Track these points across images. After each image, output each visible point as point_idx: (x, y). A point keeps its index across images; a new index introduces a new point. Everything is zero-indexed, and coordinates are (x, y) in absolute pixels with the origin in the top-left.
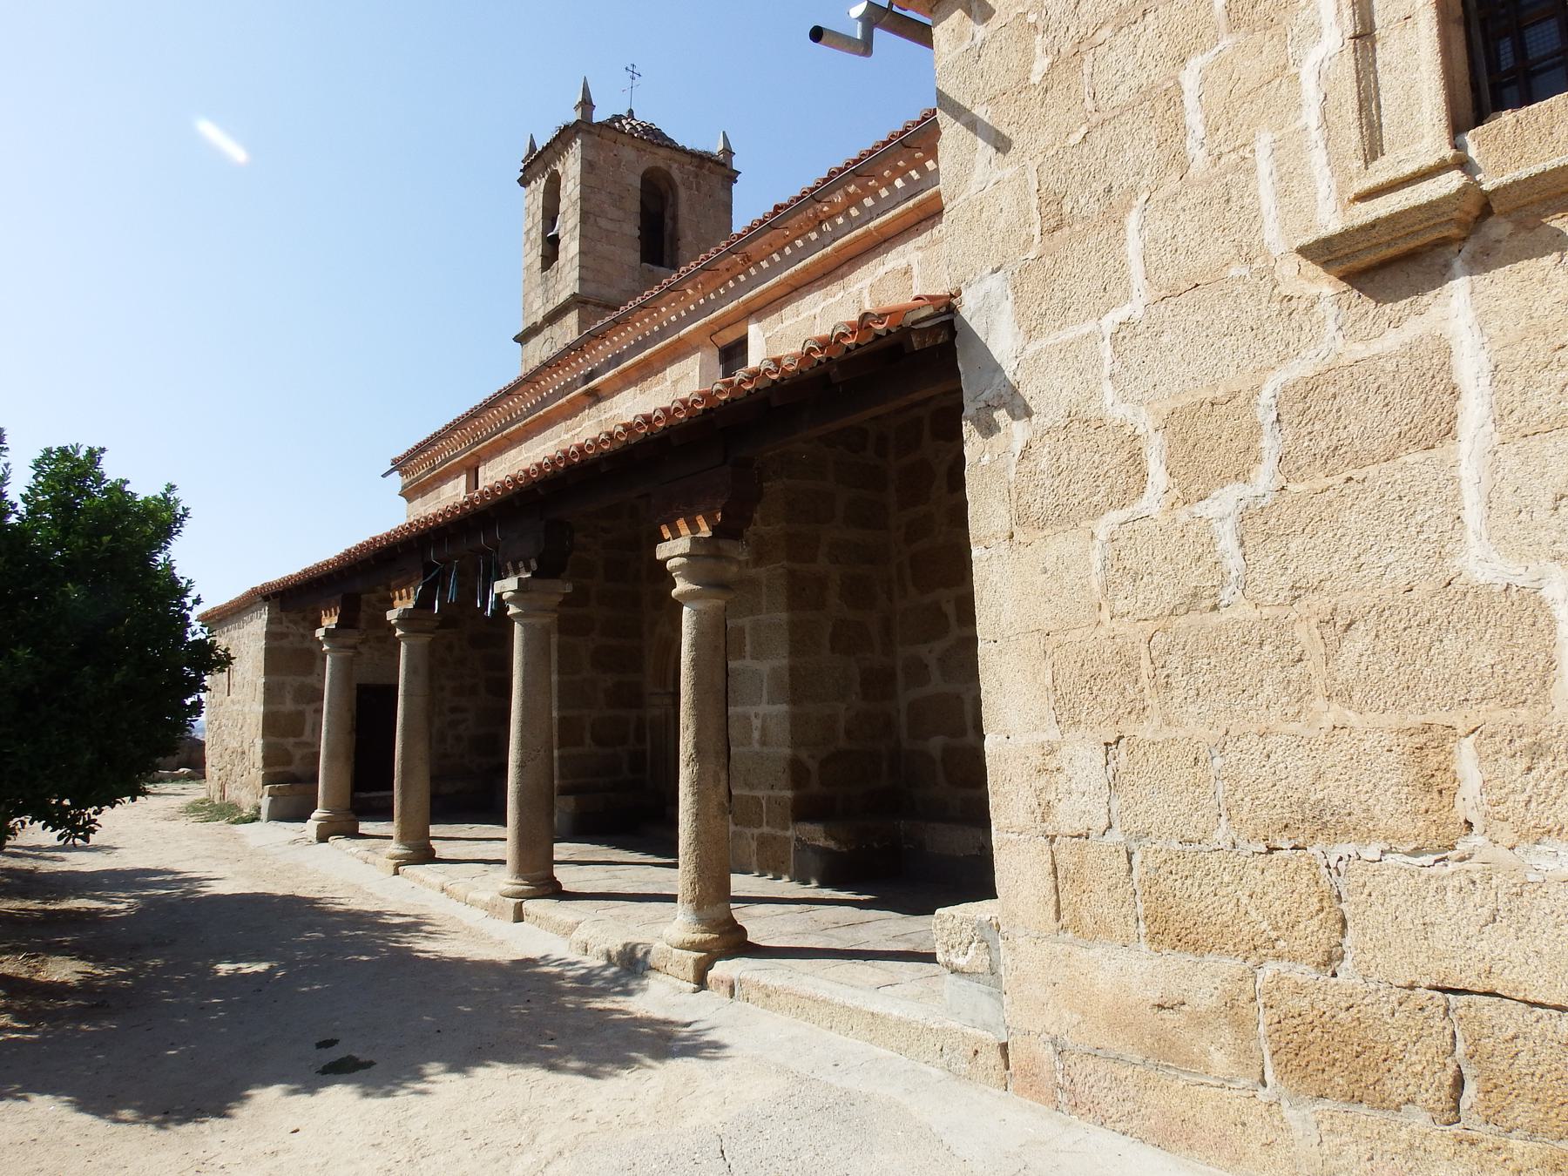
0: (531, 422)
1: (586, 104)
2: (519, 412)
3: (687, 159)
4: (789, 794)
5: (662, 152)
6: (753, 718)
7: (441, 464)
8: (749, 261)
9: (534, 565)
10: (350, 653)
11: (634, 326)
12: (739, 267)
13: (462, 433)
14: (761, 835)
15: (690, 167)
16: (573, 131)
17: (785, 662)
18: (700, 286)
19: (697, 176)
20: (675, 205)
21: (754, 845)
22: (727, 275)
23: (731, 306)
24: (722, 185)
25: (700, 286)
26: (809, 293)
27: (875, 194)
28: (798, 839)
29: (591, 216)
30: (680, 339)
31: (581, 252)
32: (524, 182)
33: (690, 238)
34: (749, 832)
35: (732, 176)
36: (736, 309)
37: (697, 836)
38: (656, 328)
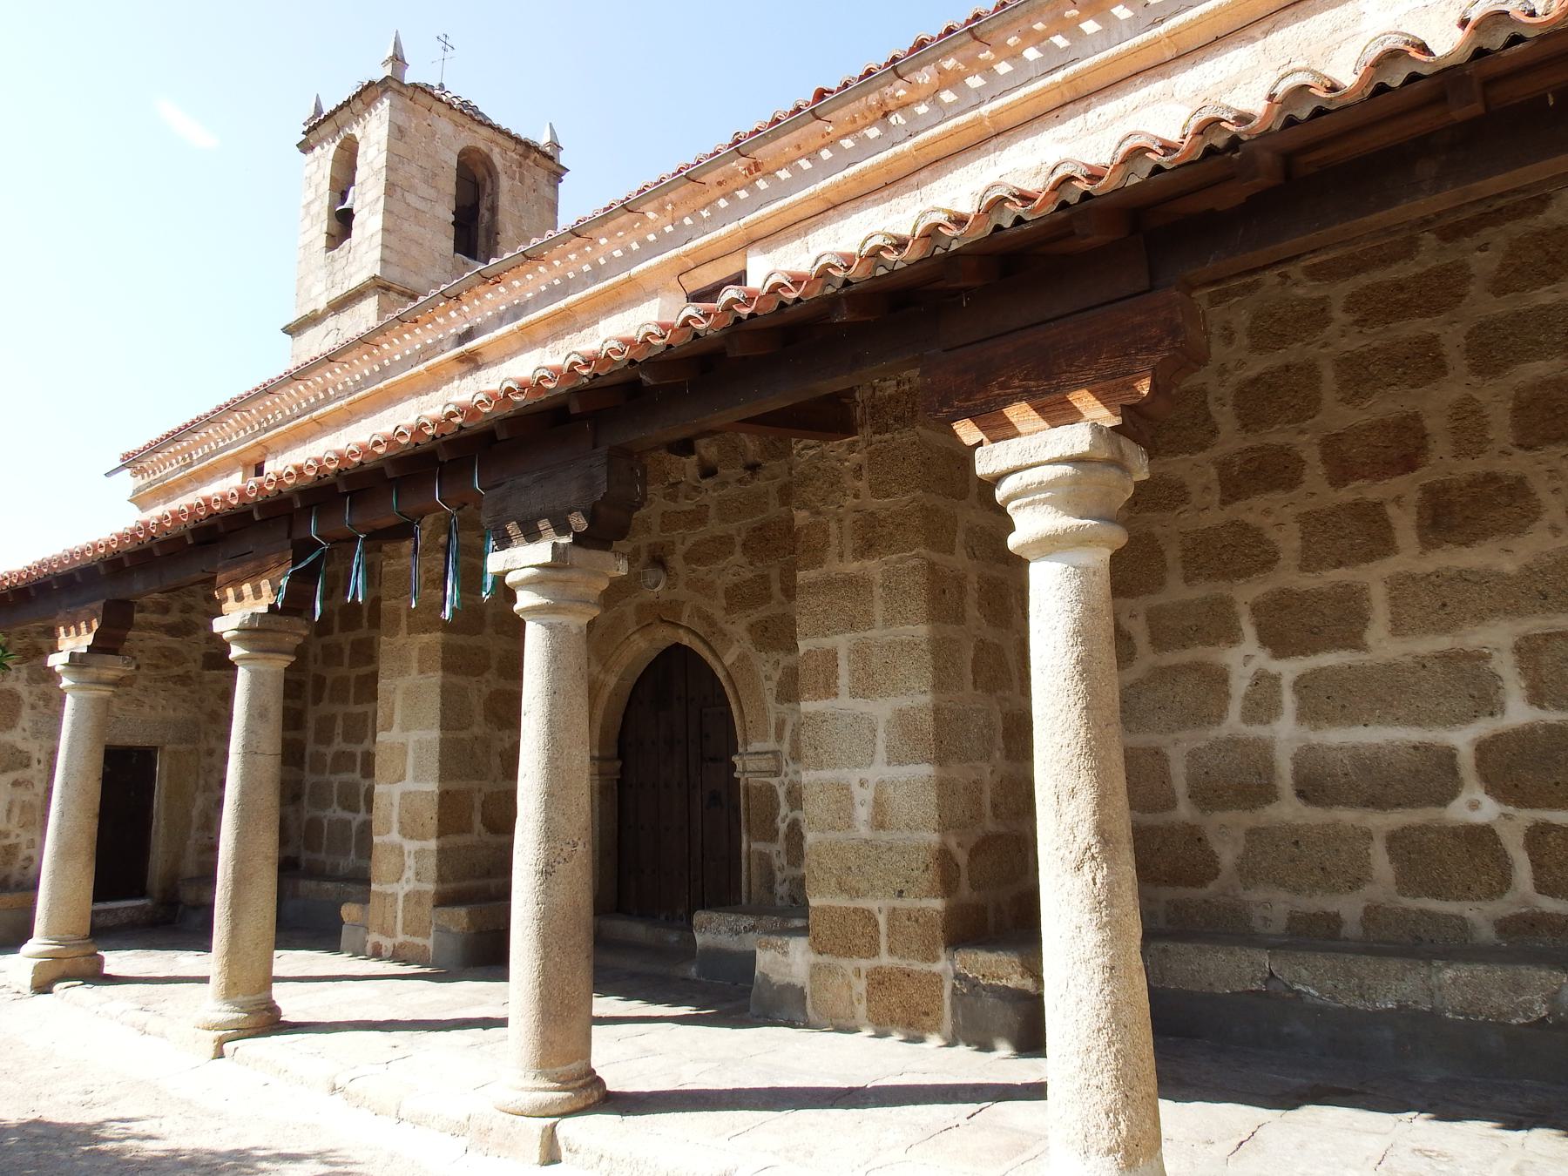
0: (360, 399)
1: (398, 60)
2: (340, 387)
3: (511, 145)
4: (937, 904)
5: (484, 132)
6: (855, 787)
7: (201, 460)
8: (757, 170)
9: (579, 522)
10: (105, 692)
11: (549, 265)
12: (741, 179)
13: (243, 418)
14: (877, 970)
15: (513, 154)
16: (380, 90)
17: (926, 700)
18: (669, 207)
19: (520, 166)
20: (495, 193)
21: (861, 986)
22: (718, 191)
23: (723, 231)
24: (548, 181)
25: (669, 207)
26: (857, 210)
27: (987, 70)
28: (957, 976)
29: (398, 189)
30: (630, 280)
31: (384, 229)
32: (305, 147)
33: (510, 234)
34: (848, 965)
35: (558, 173)
36: (731, 234)
37: (1115, 1011)
38: (586, 268)
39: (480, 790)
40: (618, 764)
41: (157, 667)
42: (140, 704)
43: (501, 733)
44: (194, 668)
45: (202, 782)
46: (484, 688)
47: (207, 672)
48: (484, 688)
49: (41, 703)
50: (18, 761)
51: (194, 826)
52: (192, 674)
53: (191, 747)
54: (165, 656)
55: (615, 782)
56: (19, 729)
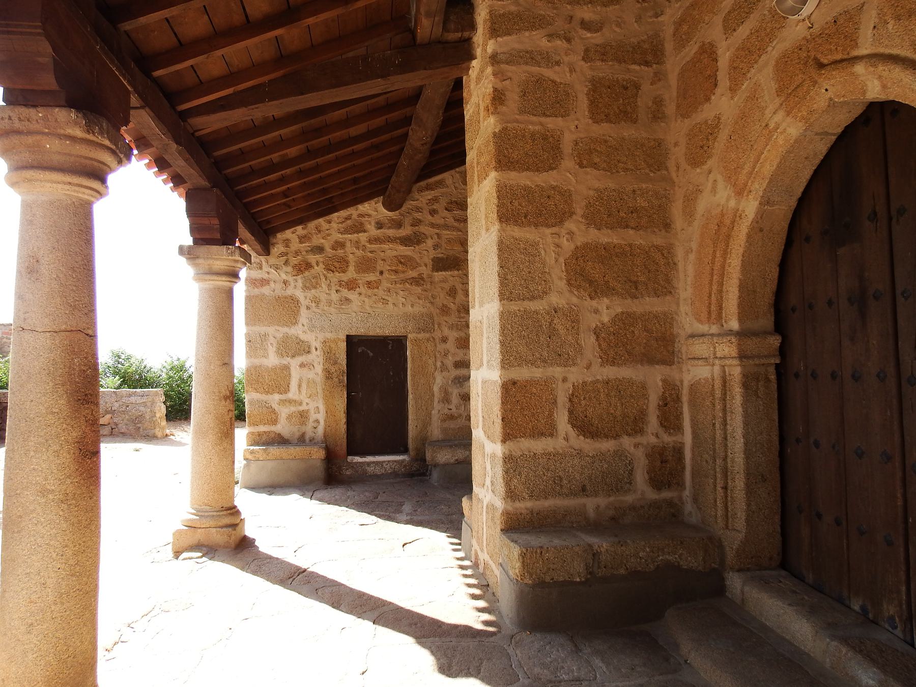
39: (565, 380)
40: (775, 341)
41: (396, 272)
42: (385, 302)
43: (594, 303)
44: (425, 271)
45: (439, 364)
46: (564, 242)
47: (436, 273)
48: (564, 242)
49: (314, 305)
50: (302, 348)
51: (436, 400)
52: (425, 276)
53: (427, 335)
54: (401, 263)
55: (772, 370)
56: (300, 325)
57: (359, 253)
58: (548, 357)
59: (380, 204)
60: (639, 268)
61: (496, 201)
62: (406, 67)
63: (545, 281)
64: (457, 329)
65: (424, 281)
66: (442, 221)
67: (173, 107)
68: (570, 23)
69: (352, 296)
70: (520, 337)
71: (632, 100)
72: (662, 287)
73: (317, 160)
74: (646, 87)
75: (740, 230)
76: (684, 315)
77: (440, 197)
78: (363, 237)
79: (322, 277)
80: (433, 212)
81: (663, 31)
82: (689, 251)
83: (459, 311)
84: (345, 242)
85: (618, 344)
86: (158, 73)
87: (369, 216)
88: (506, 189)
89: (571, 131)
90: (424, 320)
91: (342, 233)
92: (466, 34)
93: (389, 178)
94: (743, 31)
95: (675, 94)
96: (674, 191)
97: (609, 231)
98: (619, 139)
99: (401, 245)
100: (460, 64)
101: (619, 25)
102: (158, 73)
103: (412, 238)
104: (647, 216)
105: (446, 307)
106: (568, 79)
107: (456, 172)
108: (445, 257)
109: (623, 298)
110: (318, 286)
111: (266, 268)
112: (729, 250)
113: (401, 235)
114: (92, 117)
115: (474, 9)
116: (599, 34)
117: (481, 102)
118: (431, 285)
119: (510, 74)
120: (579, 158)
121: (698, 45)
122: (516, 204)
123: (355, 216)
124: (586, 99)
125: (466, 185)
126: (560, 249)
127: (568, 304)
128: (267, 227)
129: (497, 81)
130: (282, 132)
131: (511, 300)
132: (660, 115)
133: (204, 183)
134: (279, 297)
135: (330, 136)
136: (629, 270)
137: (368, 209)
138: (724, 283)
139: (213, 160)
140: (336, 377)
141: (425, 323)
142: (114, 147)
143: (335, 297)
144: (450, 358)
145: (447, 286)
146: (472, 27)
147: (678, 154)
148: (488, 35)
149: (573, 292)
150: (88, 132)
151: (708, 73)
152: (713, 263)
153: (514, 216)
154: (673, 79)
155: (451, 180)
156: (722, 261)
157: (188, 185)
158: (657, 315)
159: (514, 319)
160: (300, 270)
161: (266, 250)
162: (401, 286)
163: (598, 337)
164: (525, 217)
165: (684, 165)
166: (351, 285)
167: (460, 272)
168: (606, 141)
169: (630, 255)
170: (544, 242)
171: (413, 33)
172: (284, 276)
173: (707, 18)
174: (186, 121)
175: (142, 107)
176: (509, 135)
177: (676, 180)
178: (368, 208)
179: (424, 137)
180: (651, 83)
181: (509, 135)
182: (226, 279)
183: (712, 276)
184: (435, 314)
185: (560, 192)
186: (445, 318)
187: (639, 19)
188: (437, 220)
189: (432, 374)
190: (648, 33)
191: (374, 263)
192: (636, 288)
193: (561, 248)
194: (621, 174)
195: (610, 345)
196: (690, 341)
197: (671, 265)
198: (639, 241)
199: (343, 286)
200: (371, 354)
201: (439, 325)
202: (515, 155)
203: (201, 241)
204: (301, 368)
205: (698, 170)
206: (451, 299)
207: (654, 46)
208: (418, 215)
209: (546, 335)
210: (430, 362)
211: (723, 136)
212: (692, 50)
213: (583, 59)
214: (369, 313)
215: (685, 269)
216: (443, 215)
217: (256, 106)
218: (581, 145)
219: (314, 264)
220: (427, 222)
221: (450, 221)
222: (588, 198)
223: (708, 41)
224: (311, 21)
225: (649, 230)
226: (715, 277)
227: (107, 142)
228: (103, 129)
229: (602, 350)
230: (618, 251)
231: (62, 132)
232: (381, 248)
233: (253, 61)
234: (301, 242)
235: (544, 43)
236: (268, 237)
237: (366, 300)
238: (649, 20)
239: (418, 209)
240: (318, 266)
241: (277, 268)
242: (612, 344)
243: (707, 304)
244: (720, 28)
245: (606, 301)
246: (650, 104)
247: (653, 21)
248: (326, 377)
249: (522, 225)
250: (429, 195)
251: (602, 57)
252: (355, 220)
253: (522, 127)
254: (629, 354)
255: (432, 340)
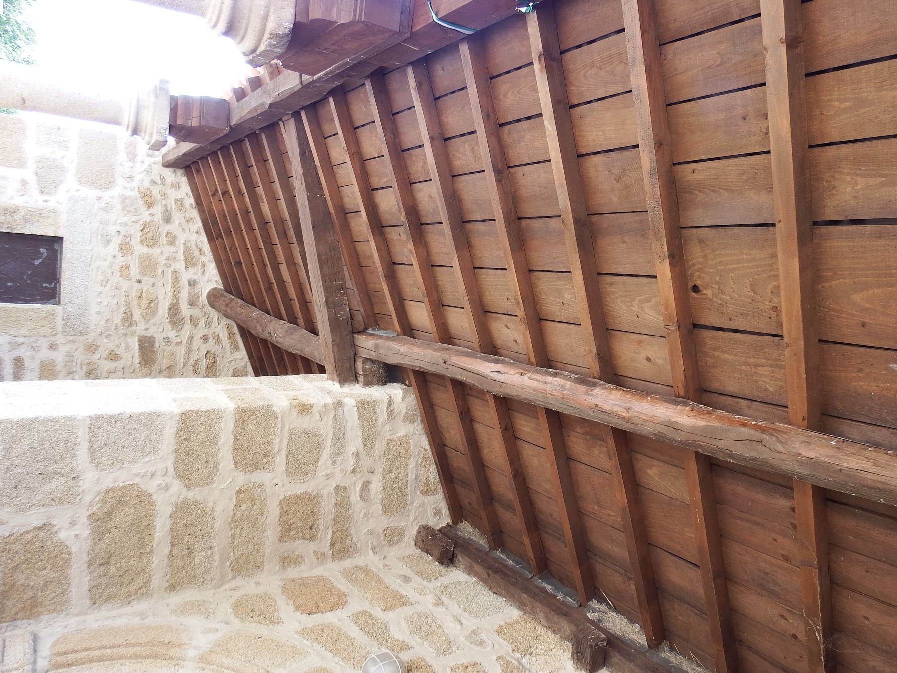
43: (84, 520)
44: (140, 328)
45: (20, 340)
46: (158, 481)
48: (158, 481)
49: (103, 205)
52: (134, 327)
53: (60, 327)
54: (150, 303)
57: (162, 260)
58: (14, 474)
59: (215, 286)
60: (125, 564)
61: (204, 409)
62: (335, 324)
63: (112, 464)
64: (67, 362)
65: (128, 327)
66: (195, 346)
67: (303, 108)
68: (368, 472)
69: (113, 248)
70: (42, 440)
71: (301, 535)
72: (102, 593)
73: (257, 230)
74: (312, 546)
75: (162, 667)
76: (66, 623)
77: (221, 346)
78: (180, 265)
79: (136, 218)
80: (205, 339)
81: (361, 556)
82: (142, 615)
83: (89, 364)
84: (175, 246)
85: (28, 553)
86: (331, 100)
87: (204, 273)
88: (216, 419)
89: (273, 479)
90: (79, 325)
91: (185, 244)
92: (361, 378)
93: (240, 296)
94: (354, 631)
95: (305, 575)
96: (211, 589)
97: (169, 527)
98: (264, 526)
99: (171, 304)
100: (336, 372)
101: (366, 515)
102: (331, 100)
103: (178, 316)
104: (184, 564)
105: (95, 350)
106: (320, 473)
107: (246, 362)
108: (156, 350)
109: (89, 551)
110: (125, 213)
111: (149, 160)
112: (140, 660)
113: (181, 304)
114: (285, 41)
115: (382, 385)
116: (359, 497)
117: (302, 392)
118: (123, 334)
119: (325, 419)
120: (246, 490)
121: (346, 590)
122: (201, 429)
123: (203, 258)
124: (302, 491)
125: (234, 375)
126: (149, 477)
127: (83, 491)
128: (193, 169)
129: (320, 408)
130: (282, 202)
131: (90, 428)
132: (286, 563)
133: (235, 120)
134: (113, 169)
135: (278, 245)
136: (123, 554)
137: (210, 272)
138: (102, 662)
139: (257, 132)
140: (7, 219)
141: (76, 326)
142: (258, 52)
143: (112, 229)
144: (29, 353)
145: (120, 351)
146: (368, 384)
147: (248, 587)
148: (359, 399)
149: (98, 495)
150: (271, 34)
151: (321, 605)
152: (126, 646)
153: (188, 428)
154: (320, 571)
155: (238, 357)
156: (128, 655)
157: (234, 102)
158: (66, 593)
159: (66, 432)
160: (145, 195)
161: (168, 164)
162: (123, 302)
163: (39, 529)
164: (186, 439)
165: (237, 595)
166: (125, 248)
167: (138, 366)
168: (262, 514)
169: (140, 553)
170: (158, 460)
171: (363, 331)
172: (138, 178)
173: (368, 595)
174: (292, 117)
175: (301, 82)
176: (269, 420)
177: (222, 589)
178: (212, 273)
179: (277, 335)
180: (316, 551)
181: (269, 420)
182: (131, 121)
183: (110, 647)
184: (86, 337)
185: (211, 473)
186: (81, 349)
187: (370, 533)
188: (197, 342)
189: (7, 331)
190: (359, 542)
191: (150, 274)
192: (100, 565)
193: (151, 478)
194: (229, 533)
195: (28, 544)
196: (29, 638)
197: (128, 599)
198: (156, 560)
199: (125, 239)
200: (37, 263)
201: (73, 342)
202: (250, 426)
203: (174, 104)
204: (21, 181)
205: (230, 610)
206: (105, 355)
207: (348, 549)
208: (202, 322)
209: (44, 469)
210: (24, 331)
211: (262, 630)
212: (342, 585)
213: (338, 486)
214: (90, 264)
215: (122, 615)
216: (201, 349)
217: (304, 184)
218: (259, 490)
219: (151, 211)
220: (194, 332)
221: (195, 356)
222: (205, 502)
223: (349, 600)
224: (372, 243)
225: (169, 569)
226: (109, 651)
227: (262, 48)
228: (274, 48)
229: (21, 535)
230: (146, 539)
231: (272, 11)
232: (168, 283)
233: (343, 188)
234: (176, 201)
235: (351, 449)
236: (184, 168)
237: (107, 263)
238: (369, 543)
239: (208, 324)
240: (150, 215)
241: (148, 172)
242: (29, 546)
243: (76, 648)
244: (358, 608)
245: (86, 532)
246: (296, 553)
247: (369, 546)
248: (7, 209)
249: (178, 435)
250: (224, 335)
251: (339, 503)
252: (199, 259)
253: (277, 432)
254: (16, 568)
255: (53, 333)
